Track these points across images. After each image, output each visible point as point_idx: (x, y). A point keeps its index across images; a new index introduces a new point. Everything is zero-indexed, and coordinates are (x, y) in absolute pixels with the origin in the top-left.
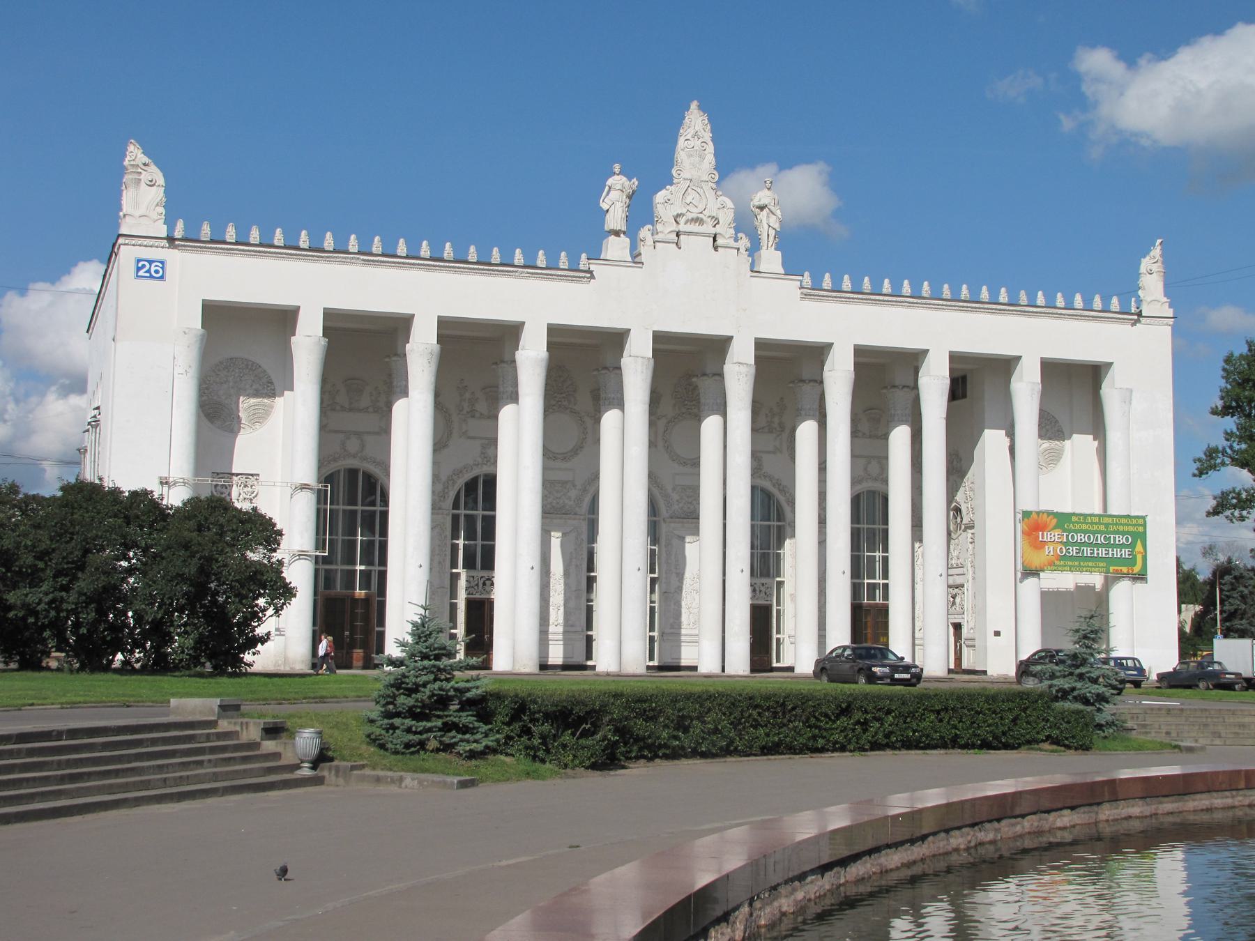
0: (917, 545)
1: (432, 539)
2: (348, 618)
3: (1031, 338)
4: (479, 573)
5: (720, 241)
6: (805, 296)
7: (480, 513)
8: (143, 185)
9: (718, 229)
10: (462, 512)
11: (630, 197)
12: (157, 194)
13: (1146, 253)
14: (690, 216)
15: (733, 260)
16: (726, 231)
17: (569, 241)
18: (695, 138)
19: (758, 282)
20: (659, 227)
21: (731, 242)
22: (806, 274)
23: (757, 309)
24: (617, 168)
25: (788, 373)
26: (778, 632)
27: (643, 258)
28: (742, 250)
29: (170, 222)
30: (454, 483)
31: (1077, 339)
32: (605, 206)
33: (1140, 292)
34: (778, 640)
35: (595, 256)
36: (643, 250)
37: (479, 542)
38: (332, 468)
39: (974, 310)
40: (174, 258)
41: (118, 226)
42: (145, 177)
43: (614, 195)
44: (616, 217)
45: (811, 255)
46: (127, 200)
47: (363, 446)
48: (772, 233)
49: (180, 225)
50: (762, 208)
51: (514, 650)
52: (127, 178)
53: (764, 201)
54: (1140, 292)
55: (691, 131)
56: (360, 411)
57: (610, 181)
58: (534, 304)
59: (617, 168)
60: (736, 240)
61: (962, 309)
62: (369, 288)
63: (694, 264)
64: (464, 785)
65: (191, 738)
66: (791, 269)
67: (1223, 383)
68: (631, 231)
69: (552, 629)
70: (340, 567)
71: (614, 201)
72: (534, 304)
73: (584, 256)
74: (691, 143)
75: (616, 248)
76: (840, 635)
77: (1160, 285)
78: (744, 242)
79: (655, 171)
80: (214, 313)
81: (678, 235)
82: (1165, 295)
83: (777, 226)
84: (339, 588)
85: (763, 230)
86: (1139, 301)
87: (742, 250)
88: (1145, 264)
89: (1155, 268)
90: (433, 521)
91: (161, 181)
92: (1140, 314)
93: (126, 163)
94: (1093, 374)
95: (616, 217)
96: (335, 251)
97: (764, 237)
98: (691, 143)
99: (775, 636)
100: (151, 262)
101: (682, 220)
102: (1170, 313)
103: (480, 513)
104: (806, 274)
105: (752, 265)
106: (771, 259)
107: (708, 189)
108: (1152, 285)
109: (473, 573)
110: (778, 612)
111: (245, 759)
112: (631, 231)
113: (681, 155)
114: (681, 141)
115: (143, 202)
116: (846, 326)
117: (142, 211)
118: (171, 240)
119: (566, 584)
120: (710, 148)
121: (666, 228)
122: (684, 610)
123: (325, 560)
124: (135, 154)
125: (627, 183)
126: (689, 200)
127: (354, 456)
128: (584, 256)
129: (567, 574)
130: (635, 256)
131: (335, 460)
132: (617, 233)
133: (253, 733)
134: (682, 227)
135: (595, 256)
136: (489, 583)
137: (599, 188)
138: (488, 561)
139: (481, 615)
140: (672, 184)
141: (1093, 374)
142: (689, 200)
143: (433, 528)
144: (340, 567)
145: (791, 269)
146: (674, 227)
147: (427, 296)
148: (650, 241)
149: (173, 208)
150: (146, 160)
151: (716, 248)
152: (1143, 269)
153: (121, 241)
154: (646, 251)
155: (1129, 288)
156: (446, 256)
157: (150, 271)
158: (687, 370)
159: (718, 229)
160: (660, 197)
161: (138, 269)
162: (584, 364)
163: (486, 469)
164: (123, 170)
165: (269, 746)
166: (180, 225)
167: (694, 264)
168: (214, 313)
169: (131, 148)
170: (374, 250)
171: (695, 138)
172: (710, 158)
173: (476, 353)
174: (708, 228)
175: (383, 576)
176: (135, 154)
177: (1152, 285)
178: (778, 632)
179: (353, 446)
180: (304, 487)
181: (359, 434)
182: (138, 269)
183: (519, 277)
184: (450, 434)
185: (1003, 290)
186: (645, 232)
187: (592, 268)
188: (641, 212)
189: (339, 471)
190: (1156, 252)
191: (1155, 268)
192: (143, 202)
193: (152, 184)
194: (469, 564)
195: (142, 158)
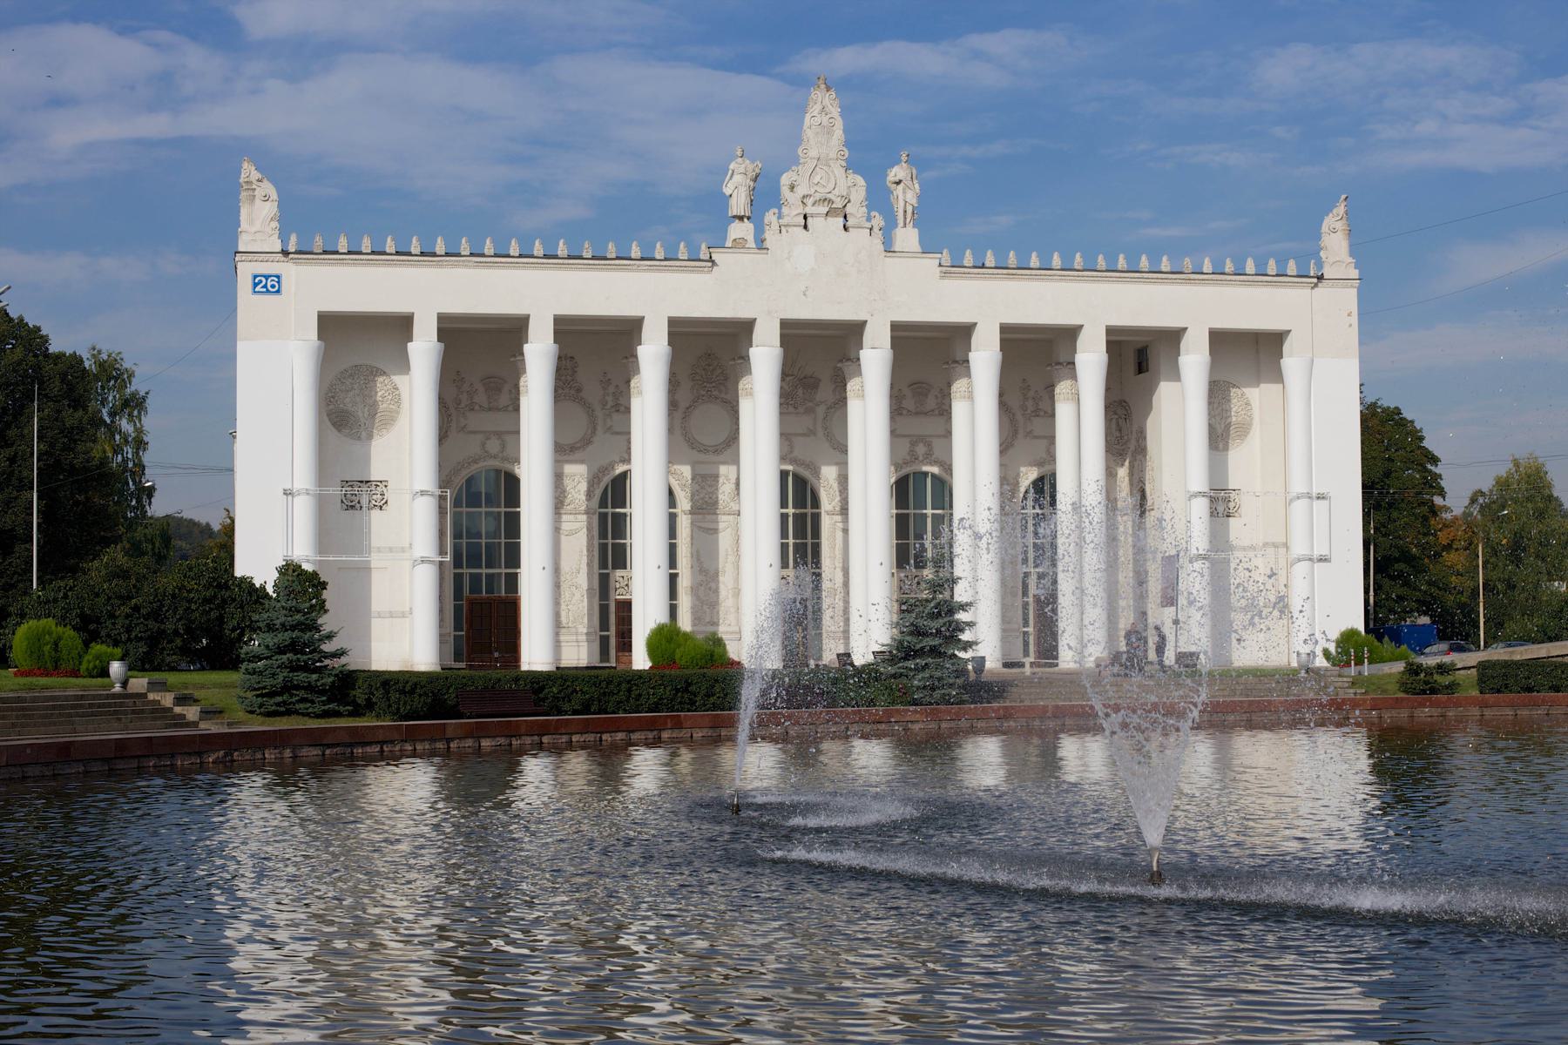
0: (754, 1025)
3: (1194, 307)
6: (944, 275)
8: (258, 201)
10: (809, 511)
14: (818, 196)
15: (863, 242)
16: (856, 210)
17: (683, 222)
19: (891, 262)
20: (785, 210)
23: (884, 282)
25: (929, 356)
27: (767, 244)
29: (284, 238)
30: (600, 481)
32: (727, 191)
34: (1026, 624)
40: (291, 272)
42: (259, 193)
43: (737, 178)
44: (739, 204)
45: (952, 233)
47: (503, 447)
48: (909, 209)
49: (293, 239)
52: (243, 195)
54: (1322, 254)
56: (499, 410)
58: (653, 297)
60: (869, 219)
63: (826, 257)
66: (927, 248)
68: (754, 216)
78: (878, 221)
80: (333, 326)
81: (805, 217)
82: (1352, 254)
86: (1320, 264)
87: (876, 230)
91: (274, 196)
92: (1320, 278)
95: (739, 204)
96: (447, 254)
100: (267, 277)
101: (810, 201)
102: (1355, 274)
103: (809, 511)
106: (907, 237)
107: (838, 171)
108: (1335, 245)
112: (754, 216)
116: (990, 303)
117: (257, 227)
118: (285, 253)
120: (839, 123)
121: (792, 213)
127: (495, 457)
130: (761, 244)
131: (475, 462)
134: (809, 210)
142: (817, 179)
146: (800, 210)
147: (541, 295)
148: (775, 226)
149: (287, 221)
151: (845, 228)
152: (1324, 228)
154: (770, 236)
156: (559, 253)
157: (268, 285)
161: (255, 285)
162: (708, 355)
165: (178, 710)
166: (293, 239)
168: (333, 326)
169: (245, 165)
170: (486, 252)
172: (839, 133)
177: (1335, 245)
179: (493, 446)
181: (499, 434)
182: (255, 285)
183: (637, 270)
184: (595, 429)
188: (765, 196)
190: (1341, 209)
191: (1340, 225)
193: (266, 199)
195: (255, 175)
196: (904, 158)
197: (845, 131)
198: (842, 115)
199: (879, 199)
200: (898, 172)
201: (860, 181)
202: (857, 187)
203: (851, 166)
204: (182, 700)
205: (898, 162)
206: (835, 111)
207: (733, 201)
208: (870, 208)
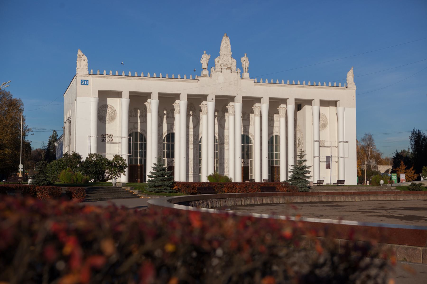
1: (158, 150)
2: (136, 171)
4: (170, 159)
6: (255, 85)
7: (170, 143)
8: (82, 60)
15: (236, 75)
16: (234, 68)
18: (226, 44)
19: (243, 81)
20: (216, 67)
22: (256, 79)
24: (205, 52)
26: (251, 174)
28: (239, 73)
36: (212, 73)
37: (170, 151)
38: (132, 132)
43: (204, 59)
45: (258, 74)
46: (78, 64)
48: (247, 68)
51: (180, 176)
52: (78, 59)
57: (203, 56)
59: (205, 52)
66: (251, 78)
67: (374, 144)
68: (209, 69)
69: (190, 173)
70: (134, 158)
71: (205, 59)
72: (183, 87)
73: (196, 76)
75: (205, 72)
76: (266, 176)
77: (353, 79)
78: (239, 71)
79: (215, 53)
84: (134, 163)
86: (347, 84)
87: (239, 73)
90: (158, 145)
92: (347, 87)
93: (78, 55)
99: (250, 175)
100: (85, 81)
102: (355, 86)
104: (256, 79)
106: (246, 75)
107: (229, 57)
108: (350, 78)
109: (169, 159)
110: (251, 168)
112: (209, 69)
115: (82, 63)
119: (193, 162)
120: (230, 46)
121: (218, 68)
122: (225, 168)
123: (130, 156)
124: (80, 53)
126: (224, 60)
128: (196, 76)
129: (194, 159)
130: (210, 75)
131: (132, 130)
135: (199, 75)
136: (173, 162)
137: (200, 58)
138: (173, 156)
139: (171, 168)
142: (224, 60)
143: (158, 147)
144: (134, 158)
151: (231, 72)
153: (77, 75)
154: (213, 74)
157: (85, 83)
160: (216, 60)
161: (82, 83)
163: (171, 132)
164: (77, 57)
166: (92, 71)
167: (224, 76)
171: (226, 44)
172: (230, 48)
173: (167, 101)
175: (145, 160)
176: (80, 53)
177: (350, 78)
178: (251, 174)
180: (124, 137)
182: (82, 83)
186: (213, 69)
188: (211, 64)
189: (133, 133)
190: (352, 70)
191: (351, 74)
192: (82, 63)
193: (85, 60)
194: (168, 157)
195: (82, 54)
197: (231, 48)
198: (230, 43)
199: (239, 65)
200: (243, 59)
201: (235, 60)
202: (234, 62)
203: (233, 56)
205: (244, 56)
207: (203, 65)
208: (237, 67)
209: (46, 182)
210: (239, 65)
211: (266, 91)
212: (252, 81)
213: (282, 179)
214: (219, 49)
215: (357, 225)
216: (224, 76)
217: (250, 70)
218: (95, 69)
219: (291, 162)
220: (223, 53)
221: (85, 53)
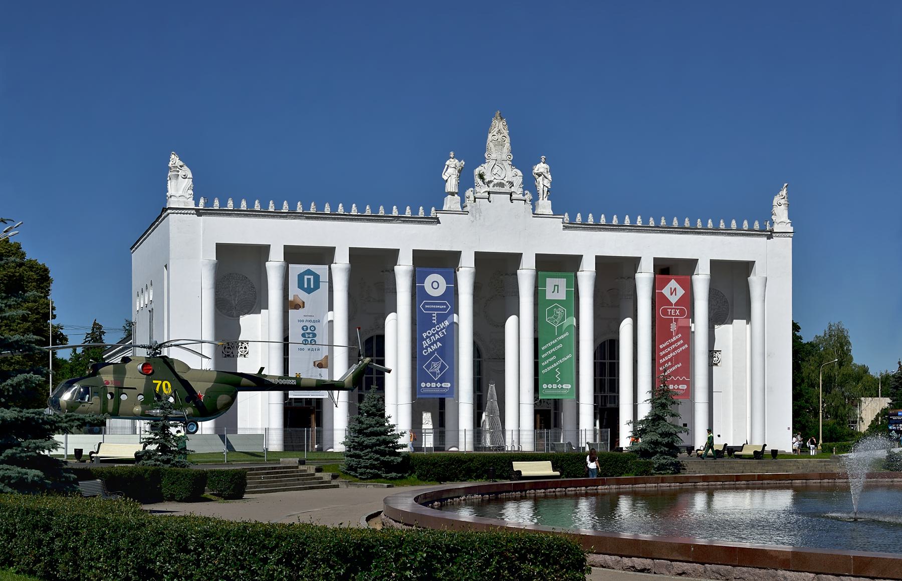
5: (514, 196)
6: (565, 228)
7: (607, 361)
9: (513, 189)
11: (459, 171)
12: (188, 183)
13: (777, 193)
14: (496, 181)
15: (523, 208)
16: (517, 190)
17: (426, 202)
18: (498, 139)
20: (477, 189)
21: (521, 196)
22: (566, 214)
31: (732, 248)
32: (445, 178)
33: (773, 217)
35: (440, 209)
39: (669, 232)
41: (166, 201)
42: (181, 173)
43: (450, 170)
44: (452, 185)
45: (571, 205)
48: (546, 189)
49: (202, 201)
50: (540, 176)
53: (541, 170)
54: (773, 217)
55: (496, 130)
57: (447, 163)
58: (404, 238)
59: (543, 157)
60: (524, 195)
61: (662, 232)
62: (617, 244)
64: (388, 486)
65: (292, 472)
66: (557, 211)
68: (461, 193)
72: (404, 238)
73: (433, 209)
74: (496, 137)
75: (452, 203)
78: (529, 196)
79: (474, 155)
80: (222, 249)
83: (548, 185)
85: (540, 188)
88: (777, 200)
89: (783, 201)
91: (190, 175)
92: (772, 231)
93: (170, 165)
94: (746, 267)
95: (452, 185)
97: (541, 192)
98: (496, 137)
101: (491, 185)
104: (566, 214)
105: (534, 209)
106: (545, 205)
107: (507, 165)
111: (311, 479)
112: (461, 193)
113: (490, 145)
114: (490, 136)
115: (180, 188)
116: (591, 245)
117: (180, 193)
120: (508, 140)
124: (175, 160)
125: (458, 164)
128: (433, 209)
132: (453, 194)
133: (311, 469)
137: (441, 167)
140: (485, 163)
141: (746, 267)
142: (495, 171)
145: (557, 211)
147: (648, 247)
148: (472, 198)
150: (181, 163)
151: (511, 200)
152: (775, 203)
154: (469, 203)
155: (767, 214)
158: (496, 271)
159: (513, 189)
163: (379, 332)
165: (318, 475)
166: (202, 201)
167: (498, 214)
168: (222, 249)
171: (498, 139)
172: (507, 145)
173: (371, 268)
174: (507, 189)
176: (175, 160)
185: (340, 205)
186: (469, 193)
187: (438, 215)
192: (180, 188)
193: (185, 177)
195: (179, 163)
196: (543, 160)
198: (509, 134)
199: (529, 184)
200: (541, 167)
201: (520, 173)
202: (515, 176)
203: (515, 164)
204: (319, 470)
206: (506, 132)
208: (524, 189)
209: (57, 413)
210: (529, 184)
211: (591, 245)
212: (558, 223)
213: (625, 441)
214: (483, 148)
215: (788, 548)
216: (498, 214)
217: (552, 194)
218: (211, 197)
219: (645, 410)
220: (494, 156)
221: (187, 160)
